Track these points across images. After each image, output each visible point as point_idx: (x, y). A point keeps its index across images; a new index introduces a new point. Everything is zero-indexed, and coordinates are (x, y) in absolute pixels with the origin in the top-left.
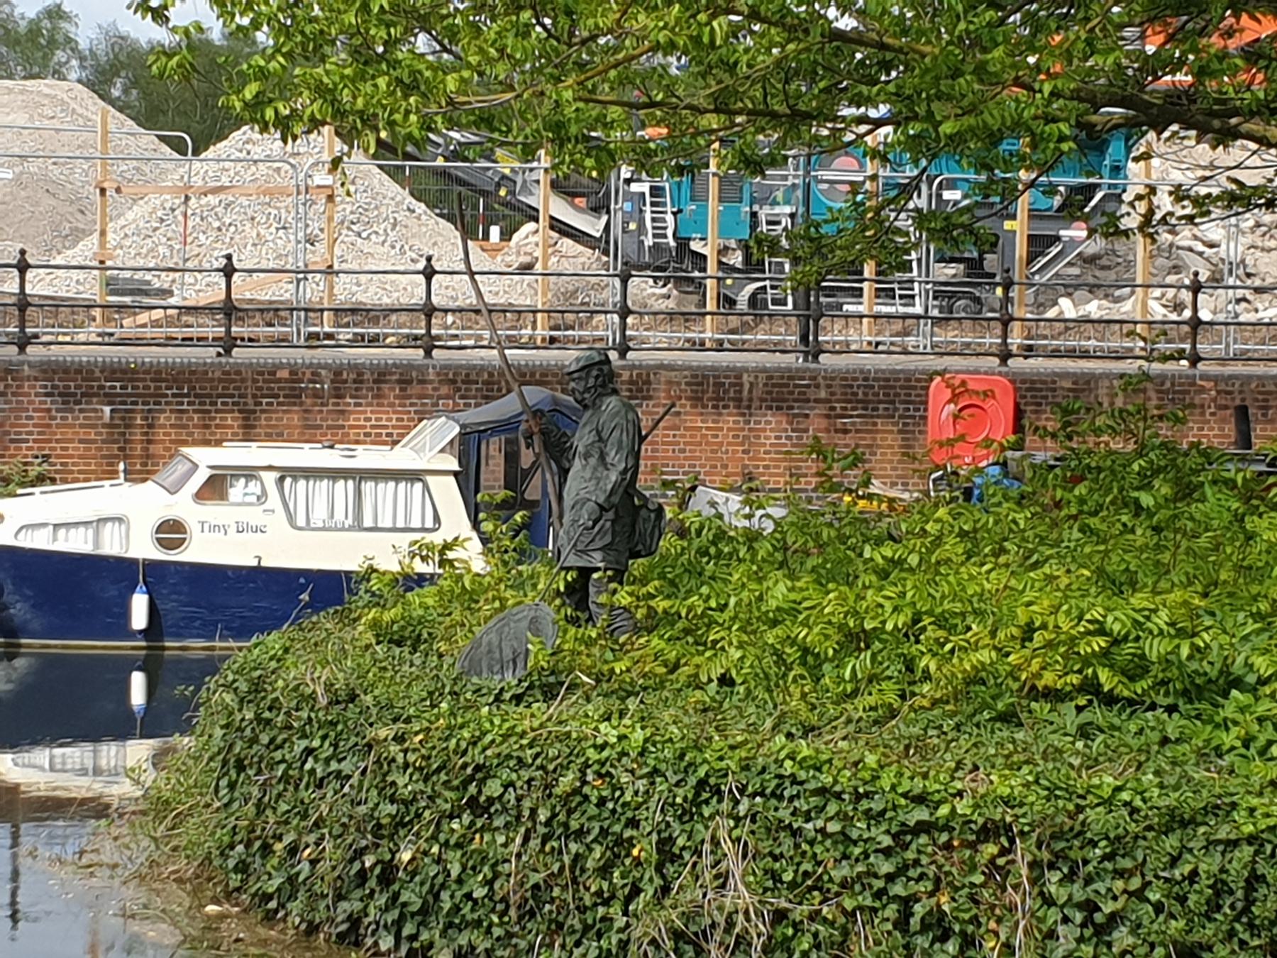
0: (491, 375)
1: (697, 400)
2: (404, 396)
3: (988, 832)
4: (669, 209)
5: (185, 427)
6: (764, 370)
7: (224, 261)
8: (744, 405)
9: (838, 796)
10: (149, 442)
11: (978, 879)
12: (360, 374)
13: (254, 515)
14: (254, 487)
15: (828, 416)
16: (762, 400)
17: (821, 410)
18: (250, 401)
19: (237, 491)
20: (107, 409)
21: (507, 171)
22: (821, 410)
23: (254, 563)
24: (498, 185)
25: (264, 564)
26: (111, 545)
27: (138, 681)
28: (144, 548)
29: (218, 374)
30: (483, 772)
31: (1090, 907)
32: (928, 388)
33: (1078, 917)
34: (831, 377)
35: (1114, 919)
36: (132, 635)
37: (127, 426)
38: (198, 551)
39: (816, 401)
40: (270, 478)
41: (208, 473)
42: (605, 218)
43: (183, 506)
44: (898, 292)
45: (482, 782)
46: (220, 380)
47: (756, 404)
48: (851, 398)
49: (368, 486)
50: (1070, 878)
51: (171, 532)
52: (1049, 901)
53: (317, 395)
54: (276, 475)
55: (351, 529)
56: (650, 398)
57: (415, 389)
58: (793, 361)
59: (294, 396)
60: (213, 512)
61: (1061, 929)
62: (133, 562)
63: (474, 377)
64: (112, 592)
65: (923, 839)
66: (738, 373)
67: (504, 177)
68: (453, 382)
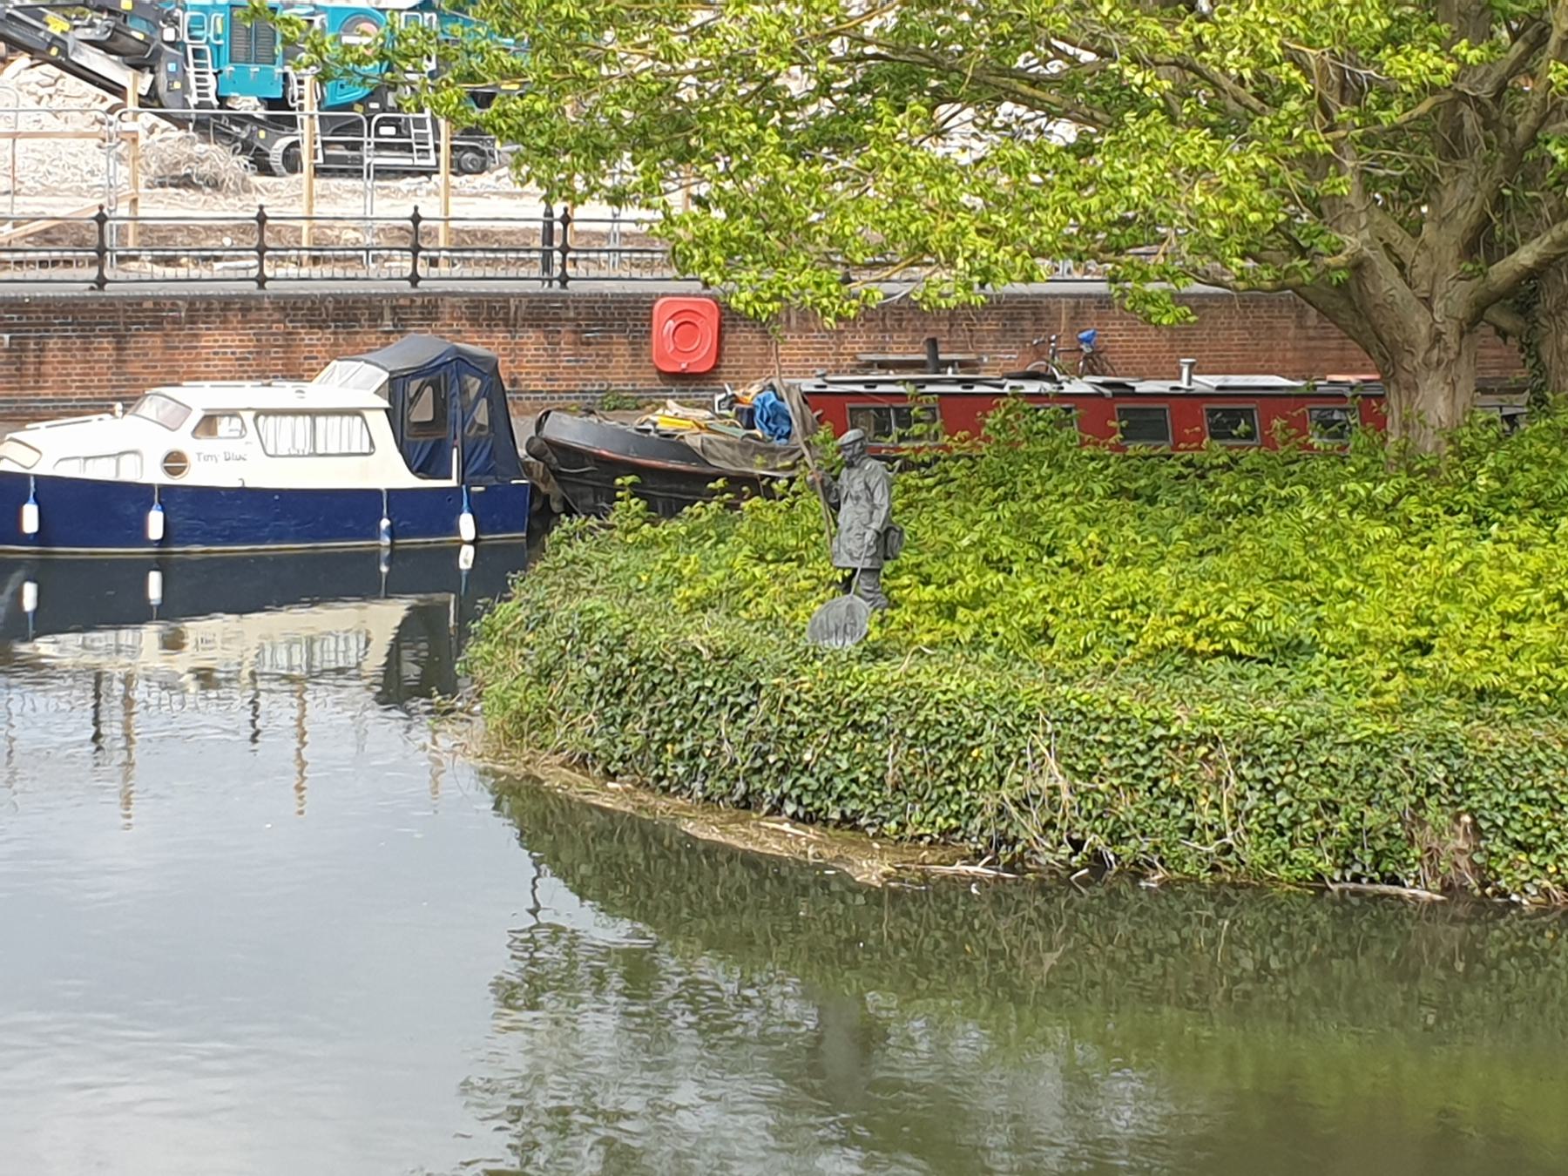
0: (313, 302)
1: (474, 320)
2: (245, 321)
3: (1201, 740)
4: (211, 70)
5: (69, 350)
6: (526, 295)
7: (97, 212)
8: (510, 324)
9: (1107, 721)
10: (41, 363)
11: (1196, 766)
12: (210, 304)
13: (236, 447)
14: (236, 422)
15: (575, 332)
16: (525, 320)
17: (570, 326)
18: (122, 327)
19: (224, 426)
20: (7, 337)
21: (58, 33)
22: (570, 326)
23: (239, 484)
24: (50, 46)
25: (248, 485)
26: (130, 473)
27: (155, 579)
28: (158, 477)
29: (96, 306)
30: (863, 706)
31: (1265, 781)
32: (651, 308)
33: (1258, 787)
34: (578, 300)
35: (1277, 788)
36: (149, 543)
37: (22, 350)
38: (194, 477)
39: (567, 320)
40: (248, 417)
41: (201, 414)
42: (149, 78)
43: (182, 440)
44: (415, 147)
45: (863, 713)
46: (98, 311)
47: (520, 322)
48: (593, 317)
49: (320, 420)
50: (1251, 766)
51: (174, 462)
52: (1242, 778)
53: (175, 321)
54: (252, 414)
55: (310, 455)
56: (437, 319)
57: (253, 315)
58: (536, 287)
59: (157, 323)
60: (207, 445)
61: (1248, 794)
62: (375, 494)
63: (299, 305)
64: (133, 509)
65: (1162, 745)
66: (506, 297)
67: (55, 38)
68: (284, 309)
